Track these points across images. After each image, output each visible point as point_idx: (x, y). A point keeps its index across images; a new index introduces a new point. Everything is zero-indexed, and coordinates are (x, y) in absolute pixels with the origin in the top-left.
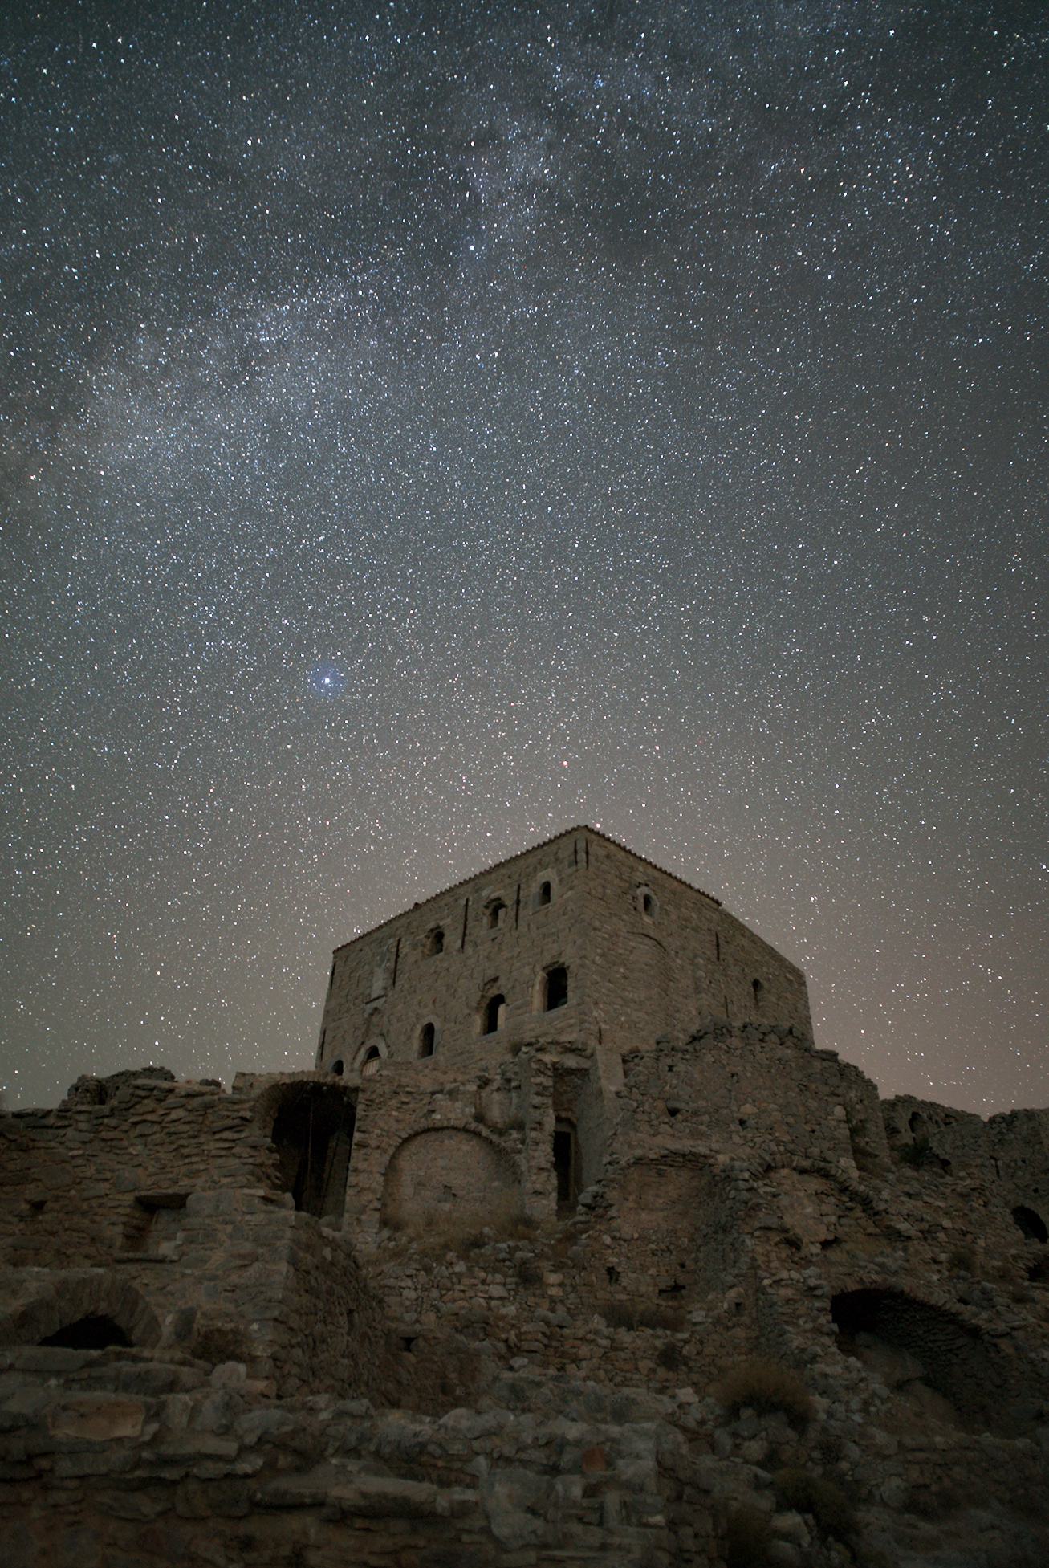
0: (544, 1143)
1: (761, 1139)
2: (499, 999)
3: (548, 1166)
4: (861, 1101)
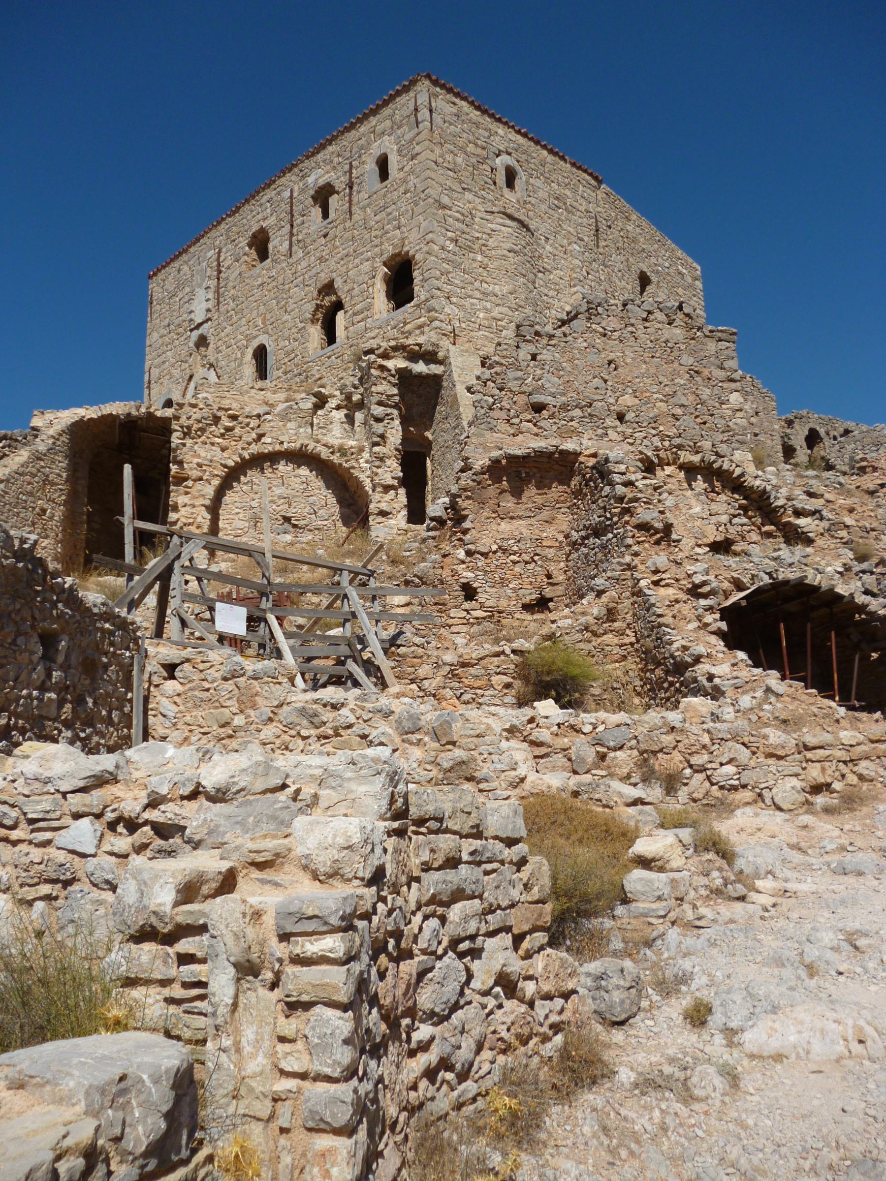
0: (389, 458)
1: (643, 434)
2: (338, 306)
3: (395, 483)
4: (757, 413)
